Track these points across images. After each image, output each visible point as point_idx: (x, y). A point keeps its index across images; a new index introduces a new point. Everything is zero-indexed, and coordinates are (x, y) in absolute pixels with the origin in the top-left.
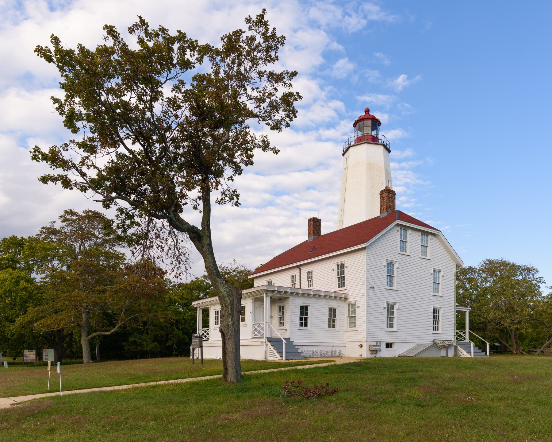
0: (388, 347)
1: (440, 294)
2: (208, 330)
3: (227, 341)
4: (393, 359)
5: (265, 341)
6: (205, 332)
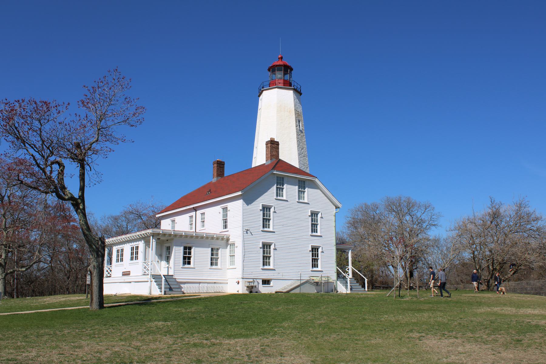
0: (265, 284)
1: (319, 234)
2: (111, 267)
3: (93, 278)
4: (270, 295)
5: (149, 278)
6: (109, 269)
